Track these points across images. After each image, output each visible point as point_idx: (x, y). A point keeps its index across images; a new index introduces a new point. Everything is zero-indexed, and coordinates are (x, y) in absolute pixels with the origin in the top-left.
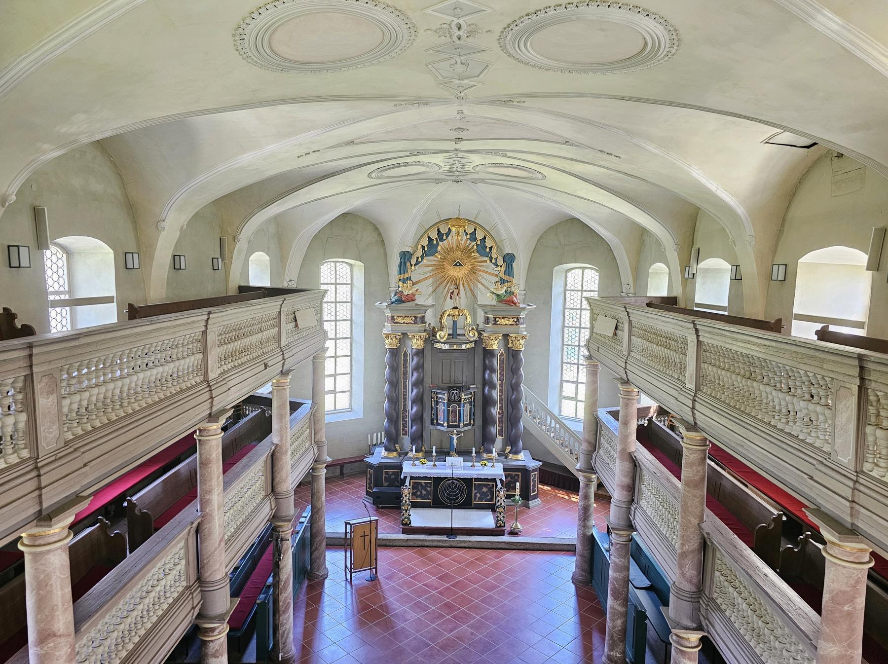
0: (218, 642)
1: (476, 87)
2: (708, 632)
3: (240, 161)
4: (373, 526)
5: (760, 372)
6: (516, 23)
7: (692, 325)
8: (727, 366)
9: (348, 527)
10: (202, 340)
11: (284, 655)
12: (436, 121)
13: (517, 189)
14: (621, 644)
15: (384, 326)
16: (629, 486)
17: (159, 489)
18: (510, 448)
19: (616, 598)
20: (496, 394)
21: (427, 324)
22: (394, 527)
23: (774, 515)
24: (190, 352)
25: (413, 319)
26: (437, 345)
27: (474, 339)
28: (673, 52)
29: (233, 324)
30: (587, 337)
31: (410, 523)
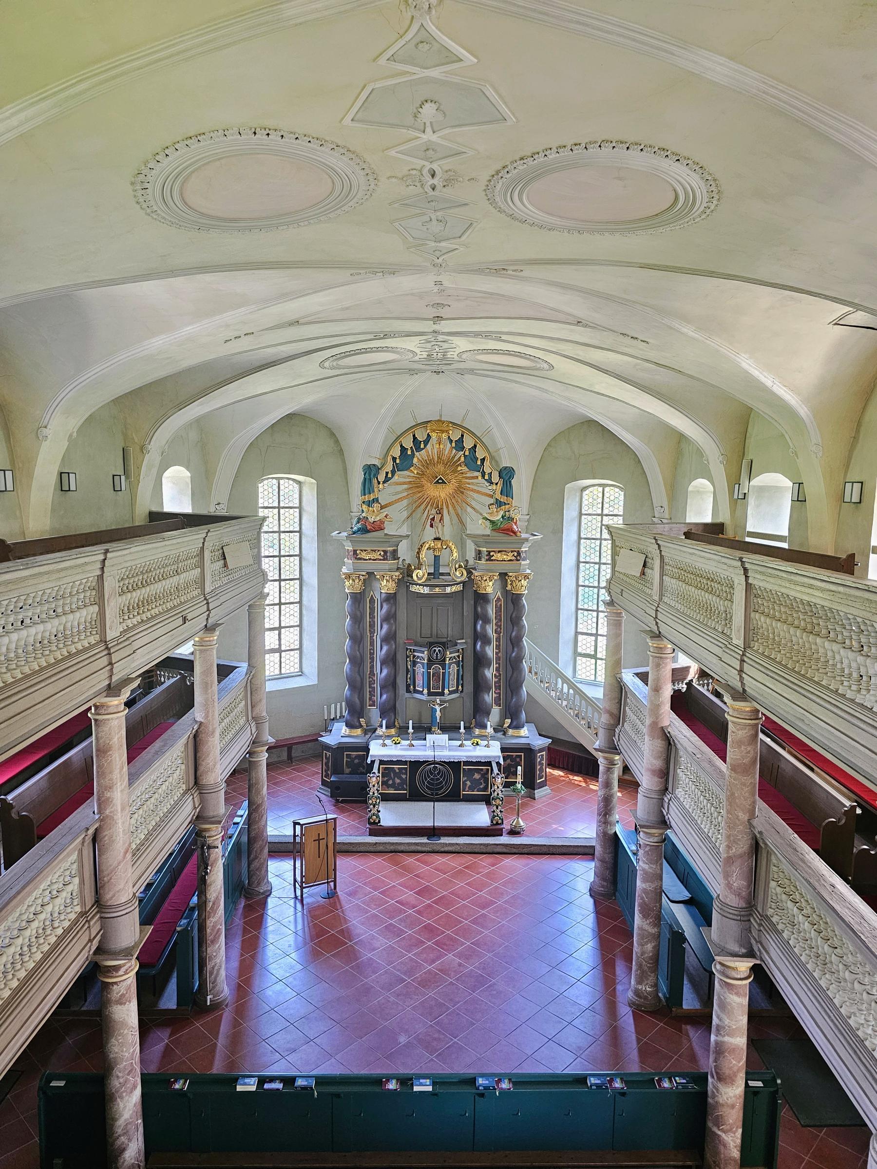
0: (125, 984)
1: (457, 251)
2: (762, 960)
3: (146, 347)
4: (330, 825)
5: (824, 624)
6: (507, 170)
7: (739, 563)
8: (784, 617)
9: (298, 827)
10: (97, 588)
11: (214, 997)
12: (407, 295)
13: (516, 382)
14: (653, 975)
15: (344, 564)
16: (661, 771)
17: (44, 784)
18: (509, 721)
19: (645, 915)
20: (490, 651)
21: (401, 560)
22: (358, 827)
23: (846, 806)
24: (80, 603)
25: (382, 553)
26: (414, 588)
27: (462, 579)
28: (712, 208)
29: (139, 566)
30: (608, 576)
31: (379, 822)
